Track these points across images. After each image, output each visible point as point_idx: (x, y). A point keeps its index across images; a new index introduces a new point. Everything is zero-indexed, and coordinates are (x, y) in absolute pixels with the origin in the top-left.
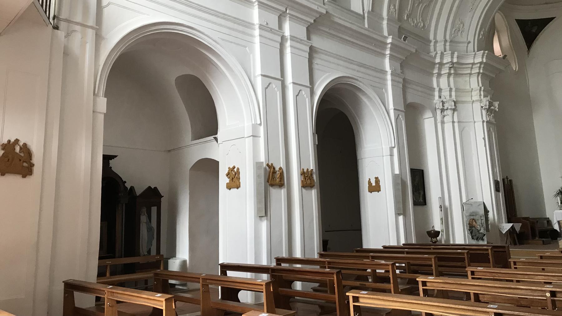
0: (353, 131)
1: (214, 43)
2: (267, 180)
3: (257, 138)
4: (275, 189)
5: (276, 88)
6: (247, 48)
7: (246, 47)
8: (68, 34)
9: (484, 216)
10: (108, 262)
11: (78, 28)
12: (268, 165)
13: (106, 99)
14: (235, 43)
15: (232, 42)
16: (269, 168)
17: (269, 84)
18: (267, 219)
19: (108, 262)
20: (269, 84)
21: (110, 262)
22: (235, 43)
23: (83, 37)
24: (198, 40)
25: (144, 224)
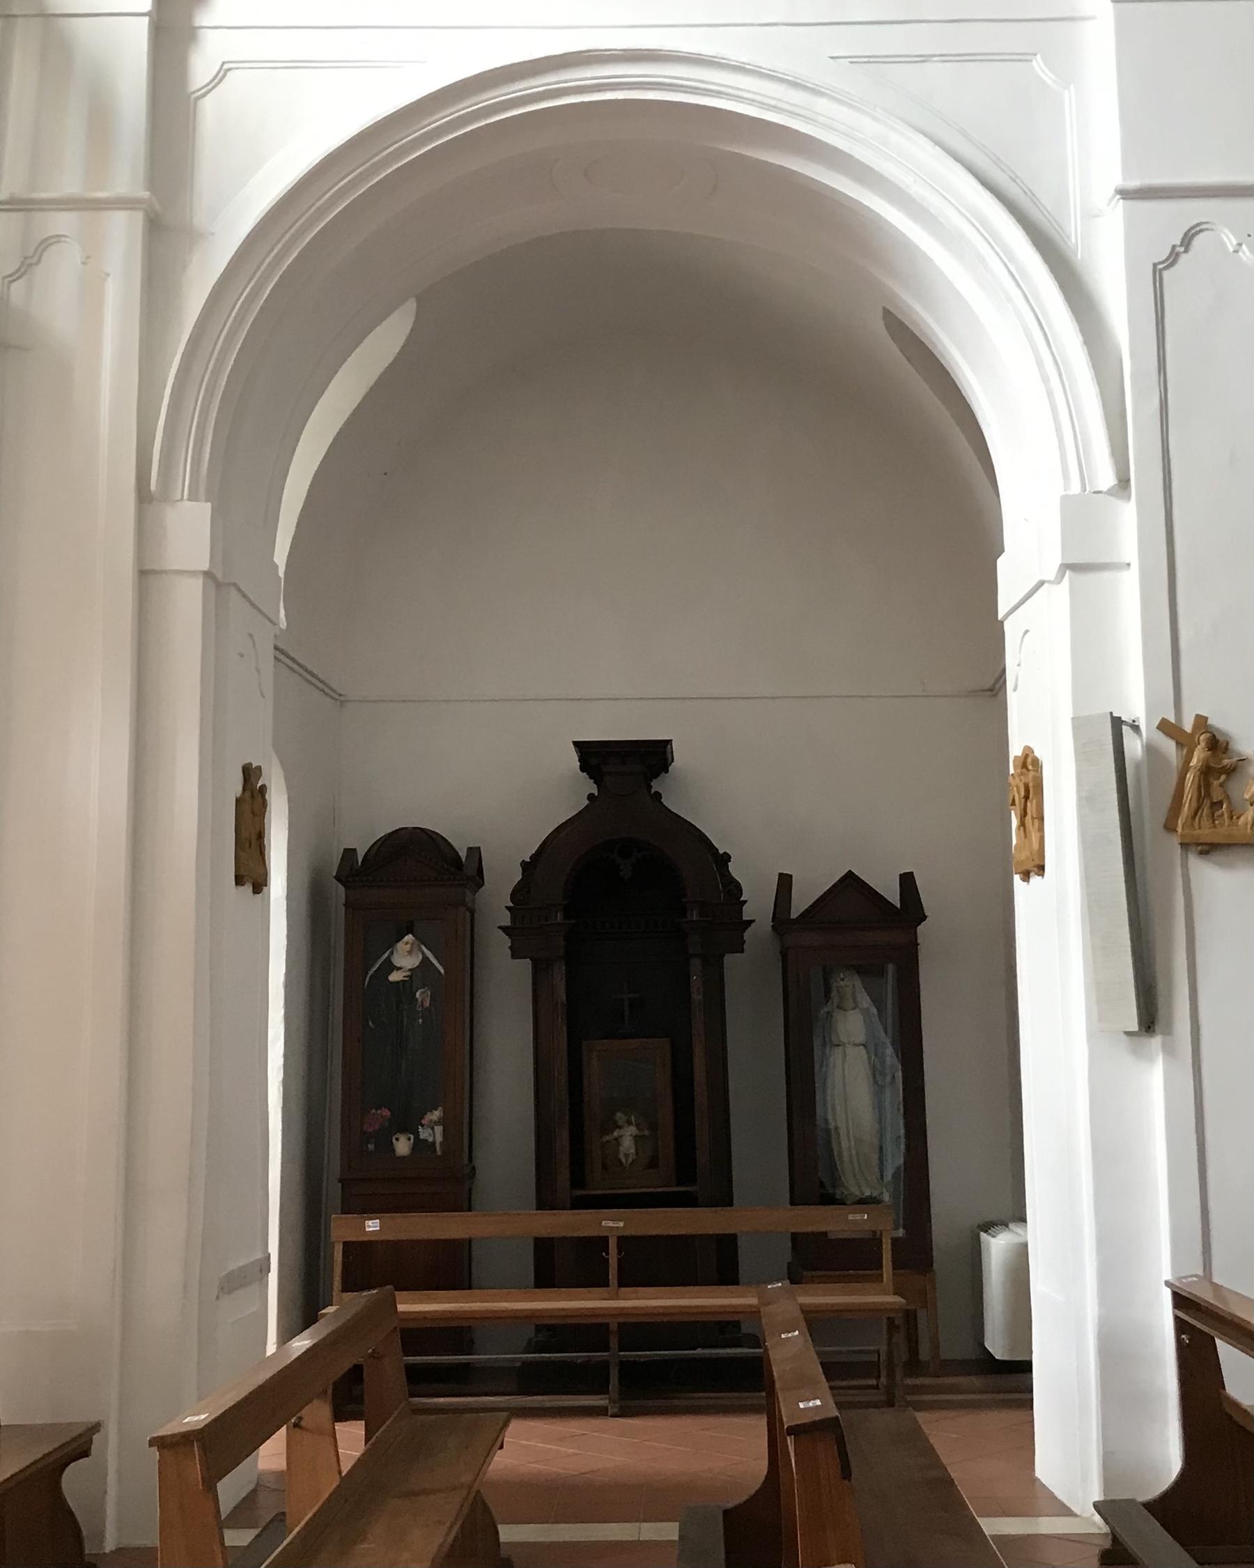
0: (994, 470)
1: (796, 97)
2: (1163, 820)
3: (1106, 575)
4: (1230, 866)
5: (1244, 247)
6: (1038, 64)
7: (1031, 61)
8: (26, 258)
9: (903, 1140)
10: (611, 1224)
11: (63, 222)
12: (1165, 727)
13: (209, 504)
14: (945, 58)
15: (925, 59)
16: (1179, 745)
17: (1187, 240)
18: (1169, 1051)
19: (611, 1224)
20: (1187, 240)
21: (621, 1224)
22: (945, 58)
23: (88, 257)
24: (698, 106)
25: (850, 1050)
